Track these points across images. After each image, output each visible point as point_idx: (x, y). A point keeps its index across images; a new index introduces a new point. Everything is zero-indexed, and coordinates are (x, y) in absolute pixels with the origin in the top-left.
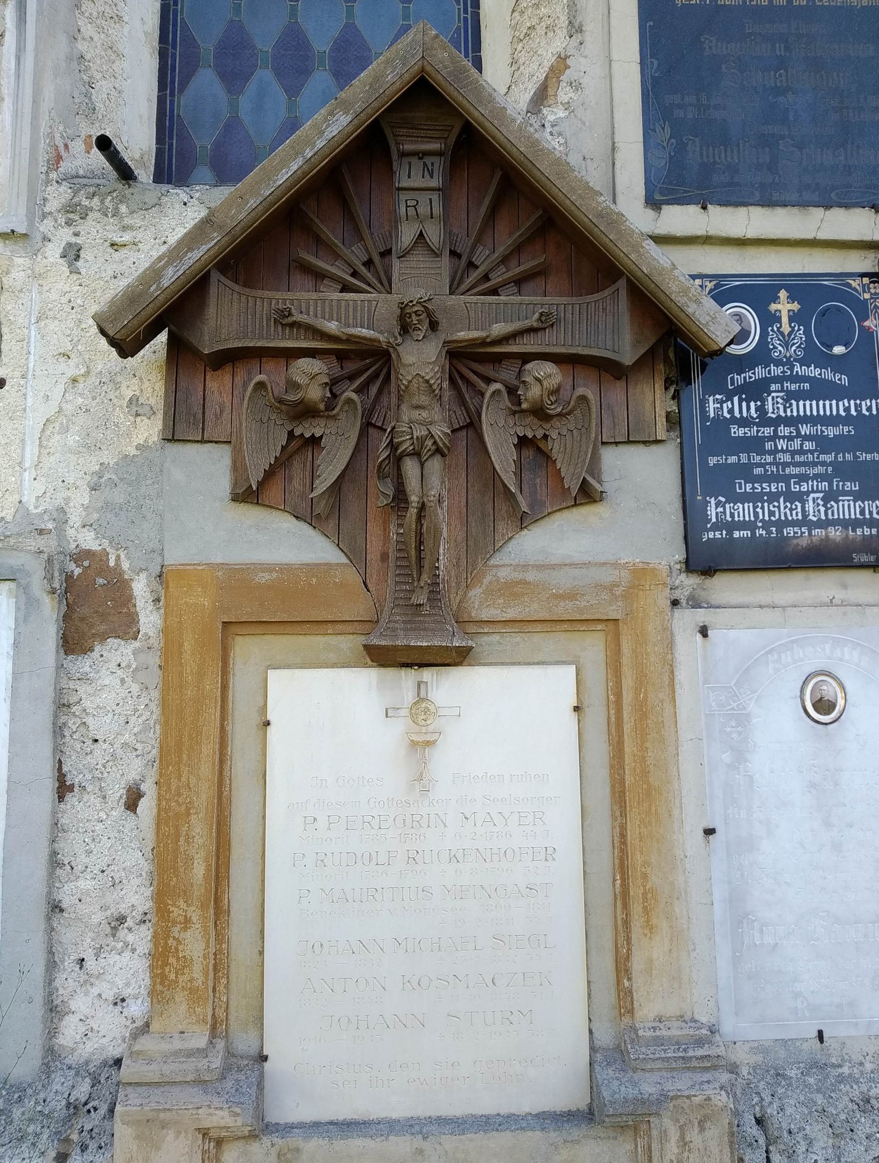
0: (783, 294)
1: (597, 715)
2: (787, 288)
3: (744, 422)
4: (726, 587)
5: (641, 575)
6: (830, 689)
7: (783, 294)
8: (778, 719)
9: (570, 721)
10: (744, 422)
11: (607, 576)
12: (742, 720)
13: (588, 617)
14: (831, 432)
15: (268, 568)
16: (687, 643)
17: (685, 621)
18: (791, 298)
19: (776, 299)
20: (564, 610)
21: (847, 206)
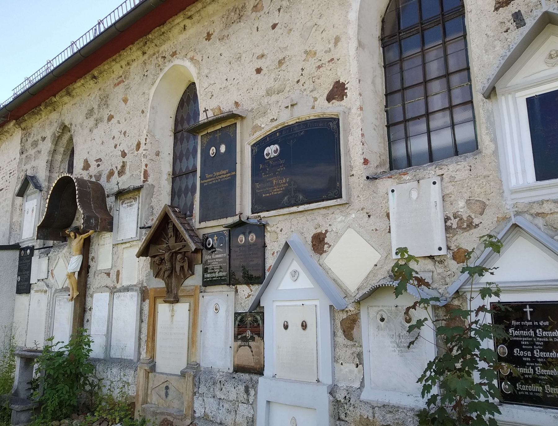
0: (528, 306)
1: (192, 311)
2: (529, 305)
3: (210, 259)
4: (209, 289)
5: (196, 287)
6: (218, 307)
7: (528, 306)
8: (211, 311)
9: (188, 312)
10: (210, 259)
11: (192, 287)
12: (206, 312)
13: (315, 359)
14: (220, 260)
15: (159, 288)
16: (201, 298)
17: (201, 294)
18: (530, 308)
19: (526, 308)
20: (188, 294)
21: (213, 220)
